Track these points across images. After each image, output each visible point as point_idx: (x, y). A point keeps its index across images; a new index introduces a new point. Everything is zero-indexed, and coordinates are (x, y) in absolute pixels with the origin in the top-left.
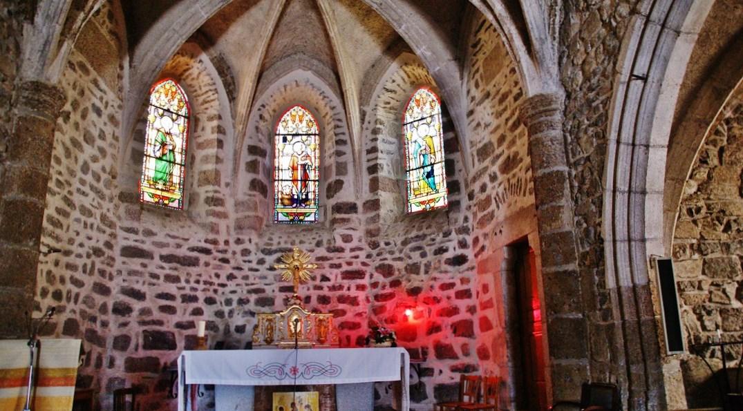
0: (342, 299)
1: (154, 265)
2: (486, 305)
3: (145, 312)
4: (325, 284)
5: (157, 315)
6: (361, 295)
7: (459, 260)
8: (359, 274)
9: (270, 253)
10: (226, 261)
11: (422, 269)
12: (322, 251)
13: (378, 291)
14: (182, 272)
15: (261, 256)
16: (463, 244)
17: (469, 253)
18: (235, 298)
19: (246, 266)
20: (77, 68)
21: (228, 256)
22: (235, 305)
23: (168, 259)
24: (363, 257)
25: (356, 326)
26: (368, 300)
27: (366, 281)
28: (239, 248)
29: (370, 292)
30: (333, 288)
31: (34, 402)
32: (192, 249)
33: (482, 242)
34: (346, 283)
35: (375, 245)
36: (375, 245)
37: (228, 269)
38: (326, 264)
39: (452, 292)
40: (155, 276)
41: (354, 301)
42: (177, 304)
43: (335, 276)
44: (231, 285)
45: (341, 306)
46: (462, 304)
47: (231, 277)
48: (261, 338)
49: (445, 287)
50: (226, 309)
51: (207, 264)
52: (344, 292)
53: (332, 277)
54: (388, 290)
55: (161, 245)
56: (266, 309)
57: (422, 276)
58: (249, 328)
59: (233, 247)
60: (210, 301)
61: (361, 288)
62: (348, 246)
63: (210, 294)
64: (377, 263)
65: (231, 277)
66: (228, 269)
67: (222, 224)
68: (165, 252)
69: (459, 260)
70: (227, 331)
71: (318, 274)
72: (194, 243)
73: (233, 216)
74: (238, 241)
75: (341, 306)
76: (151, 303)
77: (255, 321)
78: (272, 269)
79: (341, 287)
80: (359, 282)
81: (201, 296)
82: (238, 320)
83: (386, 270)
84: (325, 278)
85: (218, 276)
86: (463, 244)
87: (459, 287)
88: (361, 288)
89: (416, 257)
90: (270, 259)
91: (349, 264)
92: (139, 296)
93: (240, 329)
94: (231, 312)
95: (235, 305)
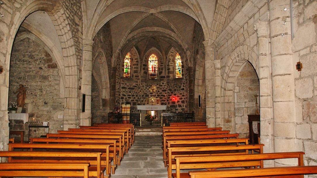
0: (162, 95)
6: (166, 95)
7: (183, 89)
16: (184, 86)
18: (141, 95)
24: (166, 87)
28: (142, 85)
30: (160, 93)
32: (133, 86)
38: (159, 88)
39: (181, 95)
45: (162, 97)
46: (183, 97)
47: (140, 91)
50: (140, 97)
54: (171, 94)
60: (137, 96)
61: (166, 93)
62: (163, 85)
65: (140, 91)
68: (129, 87)
74: (142, 84)
75: (162, 97)
77: (145, 99)
78: (148, 89)
80: (166, 92)
84: (159, 91)
85: (138, 91)
87: (183, 94)
88: (168, 93)
89: (176, 88)
91: (163, 88)
92: (125, 95)
95: (141, 96)
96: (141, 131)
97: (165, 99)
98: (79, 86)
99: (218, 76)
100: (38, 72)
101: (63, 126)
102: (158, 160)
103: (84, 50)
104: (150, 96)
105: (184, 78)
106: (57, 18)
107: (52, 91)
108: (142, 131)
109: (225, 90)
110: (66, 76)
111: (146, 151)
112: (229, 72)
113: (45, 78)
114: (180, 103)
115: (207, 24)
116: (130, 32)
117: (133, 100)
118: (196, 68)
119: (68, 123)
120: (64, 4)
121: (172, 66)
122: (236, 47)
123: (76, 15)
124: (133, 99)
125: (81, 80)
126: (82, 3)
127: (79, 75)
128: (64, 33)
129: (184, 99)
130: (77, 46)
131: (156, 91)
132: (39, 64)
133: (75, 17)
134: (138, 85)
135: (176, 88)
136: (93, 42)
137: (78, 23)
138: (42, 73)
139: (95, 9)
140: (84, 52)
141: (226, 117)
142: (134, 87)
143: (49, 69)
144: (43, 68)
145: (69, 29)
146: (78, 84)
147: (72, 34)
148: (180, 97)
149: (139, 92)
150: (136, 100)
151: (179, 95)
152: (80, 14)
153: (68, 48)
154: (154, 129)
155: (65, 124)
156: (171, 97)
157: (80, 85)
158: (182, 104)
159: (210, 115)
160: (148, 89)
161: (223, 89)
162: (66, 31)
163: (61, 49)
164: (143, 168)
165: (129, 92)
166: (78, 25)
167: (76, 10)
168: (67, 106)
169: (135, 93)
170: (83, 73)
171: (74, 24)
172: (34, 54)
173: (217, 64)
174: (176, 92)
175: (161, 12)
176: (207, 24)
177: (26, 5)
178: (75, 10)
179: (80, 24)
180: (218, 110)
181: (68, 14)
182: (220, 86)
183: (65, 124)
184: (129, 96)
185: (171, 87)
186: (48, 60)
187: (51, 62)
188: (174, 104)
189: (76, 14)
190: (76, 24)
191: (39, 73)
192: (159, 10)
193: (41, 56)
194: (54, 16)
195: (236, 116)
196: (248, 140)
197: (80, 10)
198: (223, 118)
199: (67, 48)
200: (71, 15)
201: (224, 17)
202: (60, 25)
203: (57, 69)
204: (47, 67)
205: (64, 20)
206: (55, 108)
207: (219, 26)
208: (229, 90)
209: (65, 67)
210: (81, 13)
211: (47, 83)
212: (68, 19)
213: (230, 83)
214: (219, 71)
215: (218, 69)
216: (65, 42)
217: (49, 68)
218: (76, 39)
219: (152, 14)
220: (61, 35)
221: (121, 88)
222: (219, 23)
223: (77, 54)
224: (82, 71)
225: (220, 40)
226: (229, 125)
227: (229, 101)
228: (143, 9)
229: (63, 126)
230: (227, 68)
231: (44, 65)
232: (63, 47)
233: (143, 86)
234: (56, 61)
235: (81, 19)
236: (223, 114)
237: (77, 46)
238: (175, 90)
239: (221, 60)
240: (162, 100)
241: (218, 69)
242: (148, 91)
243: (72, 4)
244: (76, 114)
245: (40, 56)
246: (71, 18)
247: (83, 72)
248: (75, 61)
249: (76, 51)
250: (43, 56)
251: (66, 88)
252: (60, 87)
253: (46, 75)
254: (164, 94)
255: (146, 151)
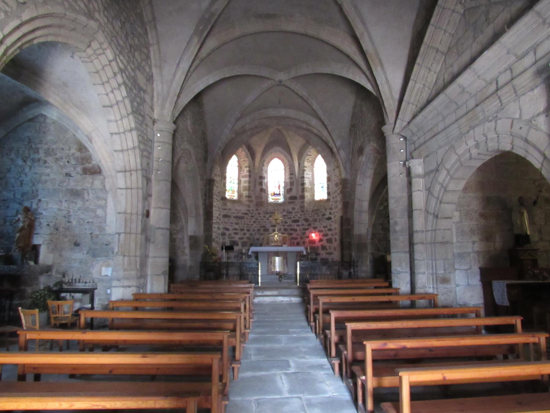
0: (292, 230)
1: (232, 220)
2: (336, 234)
3: (230, 234)
4: (286, 224)
5: (233, 235)
6: (298, 228)
7: (329, 219)
8: (297, 221)
9: (267, 213)
10: (252, 217)
11: (318, 220)
12: (285, 213)
13: (304, 227)
14: (239, 221)
15: (264, 215)
16: (330, 213)
17: (332, 216)
18: (256, 229)
19: (259, 218)
20: (243, 215)
21: (253, 215)
22: (256, 232)
23: (236, 217)
24: (299, 215)
25: (296, 239)
26: (300, 230)
27: (300, 223)
28: (257, 212)
29: (302, 227)
30: (289, 226)
31: (548, 201)
32: (243, 214)
33: (335, 214)
34: (293, 224)
35: (303, 211)
36: (303, 211)
37: (253, 219)
38: (286, 217)
39: (326, 229)
40: (232, 223)
41: (295, 230)
42: (238, 231)
43: (289, 222)
44: (255, 225)
45: (291, 232)
46: (329, 233)
47: (255, 222)
48: (265, 242)
49: (325, 227)
50: (253, 233)
51: (247, 218)
52: (292, 227)
53: (288, 222)
54: (307, 227)
55: (233, 213)
56: (267, 233)
57: (318, 223)
58: (261, 239)
59: (255, 212)
60: (248, 230)
61: (298, 226)
62: (294, 211)
63: (248, 228)
64: (304, 217)
65: (255, 222)
66: (253, 219)
67: (251, 204)
68: (235, 215)
69: (329, 219)
70: (254, 240)
71: (284, 221)
72: (243, 211)
73: (255, 201)
74: (257, 210)
75: (291, 232)
76: (231, 232)
77: (263, 237)
78: (268, 219)
79: (291, 225)
80: (298, 224)
81: (245, 229)
82: (257, 236)
83: (306, 220)
84: (286, 222)
85: (250, 222)
86: (330, 213)
87: (329, 227)
88: (303, 225)
89: (316, 217)
90: (267, 216)
91: (294, 217)
92: (227, 229)
93: (258, 239)
94: (255, 234)
95: (256, 232)
96: (260, 294)
97: (297, 236)
98: (145, 211)
99: (419, 190)
100: (63, 182)
101: (111, 291)
102: (313, 367)
103: (155, 140)
104: (271, 230)
105: (332, 200)
106: (99, 67)
107: (91, 220)
108: (263, 294)
109: (437, 217)
110: (119, 190)
111: (279, 341)
112: (447, 181)
113: (76, 194)
114: (324, 243)
115: (391, 91)
116: (239, 115)
117: (243, 238)
118: (358, 180)
119: (121, 285)
120: (115, 41)
121: (308, 178)
122: (472, 128)
123: (140, 70)
124: (242, 236)
125: (149, 199)
126: (151, 49)
127: (145, 189)
128: (114, 102)
129: (332, 235)
130: (142, 132)
131: (282, 222)
132: (64, 167)
133: (138, 73)
134: (251, 212)
135: (316, 217)
136: (174, 125)
137: (144, 88)
138: (71, 184)
139: (177, 62)
140: (156, 144)
141: (439, 272)
142: (243, 215)
143: (85, 176)
144: (73, 174)
145: (125, 94)
146: (144, 207)
147: (132, 106)
148: (324, 233)
149: (252, 223)
150: (247, 238)
151: (322, 229)
152: (147, 69)
153: (123, 133)
154: (284, 292)
155: (114, 287)
156: (307, 232)
157: (147, 208)
158: (327, 245)
159: (400, 266)
160: (268, 219)
161: (432, 216)
162: (119, 98)
163: (109, 135)
164: (288, 396)
165: (237, 224)
166: (145, 91)
167: (139, 59)
168: (120, 249)
169: (246, 226)
170: (153, 185)
171: (135, 87)
172: (54, 147)
173: (417, 166)
174: (317, 224)
175: (296, 78)
176: (391, 91)
177: (19, 17)
178: (137, 60)
179: (149, 90)
180: (421, 258)
181: (123, 63)
182: (423, 209)
183: (114, 287)
184: (234, 231)
185: (308, 214)
186: (83, 159)
187: (89, 163)
188: (314, 245)
189: (139, 68)
190: (141, 89)
191: (65, 184)
192: (293, 74)
193: (69, 150)
194: (92, 62)
195: (456, 269)
196: (546, 338)
197: (148, 63)
198: (432, 274)
199: (122, 134)
200: (129, 67)
201: (435, 73)
202: (105, 84)
203: (101, 177)
204: (81, 172)
205: (115, 74)
206: (94, 254)
207: (421, 92)
208: (446, 218)
209: (118, 172)
210: (151, 69)
211: (80, 203)
212: (124, 74)
213: (448, 203)
214: (421, 181)
215: (419, 176)
216: (116, 121)
217: (85, 174)
218: (140, 118)
219: (280, 81)
220: (108, 106)
221: (221, 216)
222: (422, 86)
223: (142, 147)
224: (153, 181)
225: (426, 118)
226: (446, 288)
227: (445, 240)
228: (264, 72)
229: (111, 291)
230: (444, 173)
231: (75, 168)
232: (114, 132)
233: (259, 214)
234: (100, 162)
235: (150, 79)
236: (433, 267)
237: (142, 132)
238: (315, 220)
239: (424, 158)
240: (293, 238)
241: (419, 176)
242: (267, 221)
243: (131, 46)
244: (138, 267)
245: (68, 152)
246: (129, 73)
247: (154, 183)
248: (139, 160)
249: (140, 142)
250: (73, 151)
251: (119, 213)
252: (106, 213)
253: (79, 188)
254: (295, 227)
255: (279, 341)
